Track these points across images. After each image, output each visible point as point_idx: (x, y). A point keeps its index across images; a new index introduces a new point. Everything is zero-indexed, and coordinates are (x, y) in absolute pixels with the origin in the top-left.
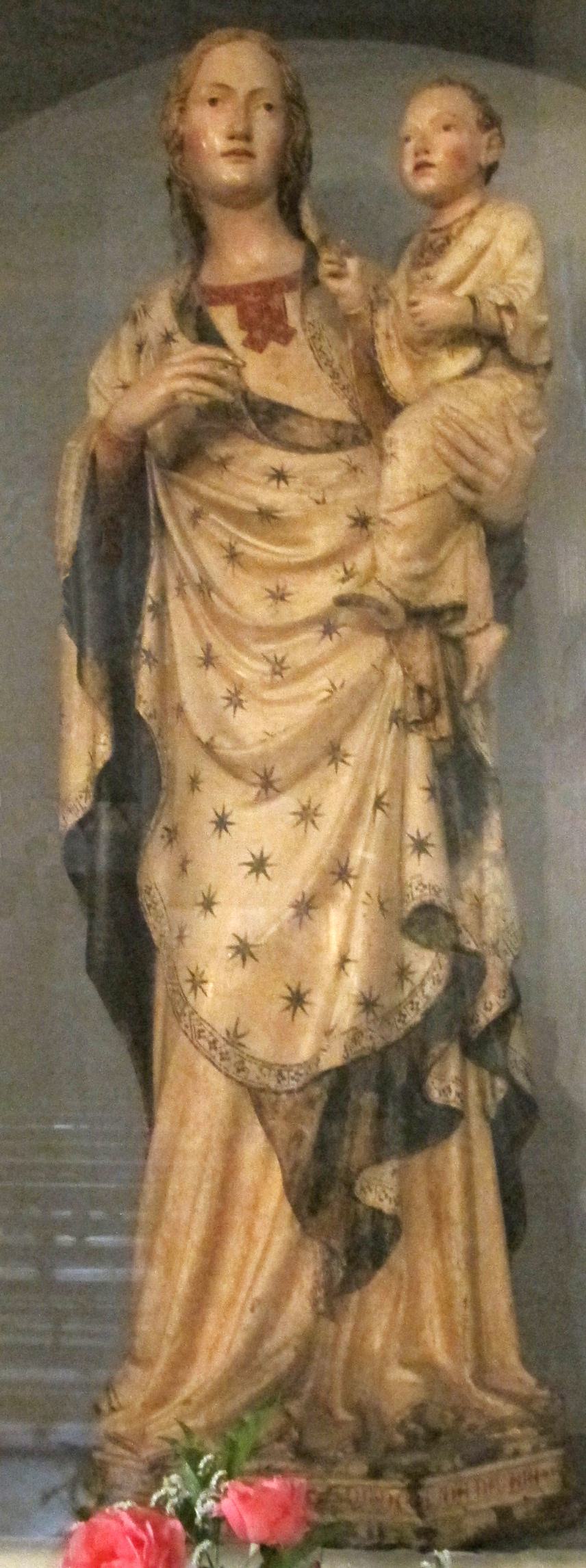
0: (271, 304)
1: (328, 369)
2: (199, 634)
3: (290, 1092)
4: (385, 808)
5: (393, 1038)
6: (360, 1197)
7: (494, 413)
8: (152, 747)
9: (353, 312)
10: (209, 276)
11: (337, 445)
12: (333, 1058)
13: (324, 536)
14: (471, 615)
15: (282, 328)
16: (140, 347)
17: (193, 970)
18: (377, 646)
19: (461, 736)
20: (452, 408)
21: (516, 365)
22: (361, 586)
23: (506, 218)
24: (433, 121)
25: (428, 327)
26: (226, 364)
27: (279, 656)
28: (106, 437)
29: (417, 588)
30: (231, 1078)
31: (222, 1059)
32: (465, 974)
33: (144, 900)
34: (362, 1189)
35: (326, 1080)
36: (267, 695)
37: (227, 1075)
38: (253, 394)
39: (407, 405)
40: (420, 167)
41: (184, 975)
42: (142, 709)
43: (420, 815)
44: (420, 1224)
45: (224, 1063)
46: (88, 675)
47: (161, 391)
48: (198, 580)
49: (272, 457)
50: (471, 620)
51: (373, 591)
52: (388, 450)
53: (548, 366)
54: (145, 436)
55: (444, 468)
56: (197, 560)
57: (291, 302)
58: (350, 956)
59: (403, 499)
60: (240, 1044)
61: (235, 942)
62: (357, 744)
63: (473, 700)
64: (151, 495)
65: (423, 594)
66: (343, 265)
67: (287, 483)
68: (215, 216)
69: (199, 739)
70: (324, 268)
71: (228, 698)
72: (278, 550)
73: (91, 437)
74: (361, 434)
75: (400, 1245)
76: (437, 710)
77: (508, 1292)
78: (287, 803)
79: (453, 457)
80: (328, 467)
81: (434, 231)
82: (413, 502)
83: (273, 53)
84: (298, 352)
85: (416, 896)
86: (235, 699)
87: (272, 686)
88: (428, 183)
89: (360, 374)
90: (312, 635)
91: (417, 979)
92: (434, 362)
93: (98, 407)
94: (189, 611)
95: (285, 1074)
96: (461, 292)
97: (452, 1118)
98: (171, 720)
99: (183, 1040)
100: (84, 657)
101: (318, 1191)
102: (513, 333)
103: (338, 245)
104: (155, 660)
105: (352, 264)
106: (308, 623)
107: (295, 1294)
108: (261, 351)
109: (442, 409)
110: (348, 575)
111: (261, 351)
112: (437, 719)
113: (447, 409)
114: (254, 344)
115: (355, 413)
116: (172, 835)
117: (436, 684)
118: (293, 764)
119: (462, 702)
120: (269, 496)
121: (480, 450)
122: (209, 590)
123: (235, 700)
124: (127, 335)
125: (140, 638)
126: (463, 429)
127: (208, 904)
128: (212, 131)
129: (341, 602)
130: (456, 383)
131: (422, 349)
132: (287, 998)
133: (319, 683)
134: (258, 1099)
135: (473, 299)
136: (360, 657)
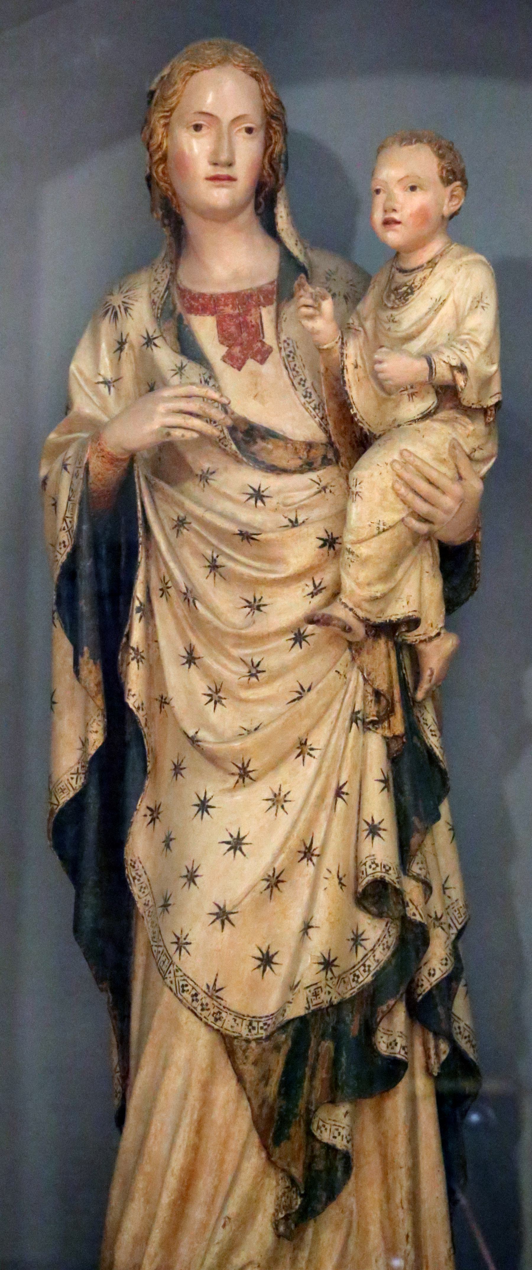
0: (249, 318)
2: (182, 633)
3: (258, 1040)
4: (344, 796)
5: (348, 996)
6: (317, 1134)
7: (445, 456)
9: (325, 347)
11: (309, 466)
12: (297, 1009)
14: (420, 630)
15: (259, 344)
16: (121, 345)
17: (178, 933)
19: (413, 728)
27: (256, 661)
30: (210, 1026)
31: (202, 1010)
32: (412, 940)
33: (130, 872)
34: (318, 1128)
35: (290, 1029)
36: (244, 694)
37: (206, 1024)
39: (376, 438)
40: (387, 223)
41: (169, 938)
42: (132, 702)
43: (378, 805)
44: (368, 1168)
45: (205, 1013)
46: (84, 673)
48: (184, 590)
51: (339, 612)
52: (354, 489)
55: (400, 506)
57: (267, 314)
58: (313, 923)
60: (218, 997)
61: (216, 910)
62: (317, 740)
64: (139, 503)
65: (382, 611)
67: (263, 502)
69: (185, 733)
75: (351, 1185)
76: (390, 711)
77: (448, 1238)
78: (261, 791)
79: (410, 496)
80: (297, 488)
84: (271, 370)
85: (370, 874)
86: (215, 697)
87: (249, 686)
91: (369, 945)
95: (255, 1024)
97: (394, 1071)
99: (167, 996)
100: (82, 655)
101: (279, 1123)
106: (280, 633)
107: (260, 1217)
108: (239, 369)
111: (239, 369)
112: (391, 719)
113: (405, 453)
116: (154, 814)
118: (267, 758)
125: (128, 636)
127: (191, 877)
132: (259, 959)
134: (229, 1045)
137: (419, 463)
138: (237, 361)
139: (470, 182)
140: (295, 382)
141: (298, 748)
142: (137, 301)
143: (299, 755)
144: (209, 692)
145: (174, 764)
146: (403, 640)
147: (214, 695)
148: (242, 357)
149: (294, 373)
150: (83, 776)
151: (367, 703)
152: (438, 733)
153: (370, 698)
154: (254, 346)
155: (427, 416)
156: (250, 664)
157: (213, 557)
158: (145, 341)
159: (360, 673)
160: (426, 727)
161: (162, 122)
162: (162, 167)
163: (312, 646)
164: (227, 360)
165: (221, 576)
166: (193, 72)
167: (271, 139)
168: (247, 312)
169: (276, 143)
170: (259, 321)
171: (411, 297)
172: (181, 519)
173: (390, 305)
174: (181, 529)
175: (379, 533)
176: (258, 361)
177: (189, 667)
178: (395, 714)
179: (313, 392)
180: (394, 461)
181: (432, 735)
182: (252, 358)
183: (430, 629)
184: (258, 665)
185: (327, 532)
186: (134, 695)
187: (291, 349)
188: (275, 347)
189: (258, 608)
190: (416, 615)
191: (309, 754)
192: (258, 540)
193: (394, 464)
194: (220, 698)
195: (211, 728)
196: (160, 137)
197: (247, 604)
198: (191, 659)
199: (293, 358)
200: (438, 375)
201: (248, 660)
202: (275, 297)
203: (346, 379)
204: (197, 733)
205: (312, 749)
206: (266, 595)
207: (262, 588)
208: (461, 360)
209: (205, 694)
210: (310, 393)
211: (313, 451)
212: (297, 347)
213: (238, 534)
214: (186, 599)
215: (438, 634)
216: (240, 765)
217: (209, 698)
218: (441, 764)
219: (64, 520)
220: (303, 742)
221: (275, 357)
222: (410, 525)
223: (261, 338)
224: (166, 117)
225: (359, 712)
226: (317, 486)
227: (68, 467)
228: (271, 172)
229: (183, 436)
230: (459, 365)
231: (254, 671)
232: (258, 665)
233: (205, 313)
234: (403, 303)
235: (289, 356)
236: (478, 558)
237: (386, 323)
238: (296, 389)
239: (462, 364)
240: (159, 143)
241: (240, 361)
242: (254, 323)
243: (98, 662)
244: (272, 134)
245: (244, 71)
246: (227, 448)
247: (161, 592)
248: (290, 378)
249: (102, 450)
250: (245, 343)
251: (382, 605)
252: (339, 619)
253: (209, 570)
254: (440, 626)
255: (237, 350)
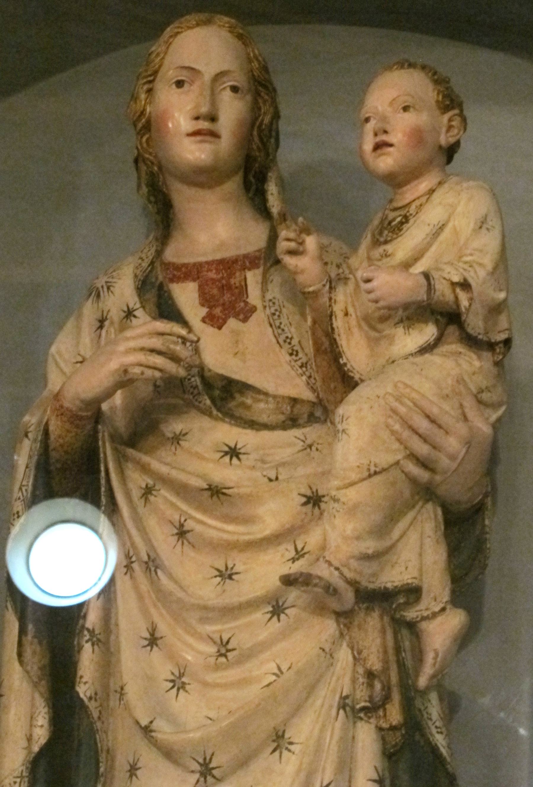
0: (232, 281)
1: (287, 346)
2: (145, 612)
8: (92, 732)
9: (311, 289)
10: (171, 254)
11: (292, 422)
13: (275, 512)
14: (422, 605)
16: (102, 322)
18: (329, 627)
19: (413, 723)
20: (406, 386)
21: (472, 342)
22: (311, 565)
23: (464, 196)
24: (396, 102)
25: (381, 304)
26: (184, 340)
28: (60, 411)
29: (368, 568)
38: (210, 370)
39: (362, 381)
42: (83, 690)
47: (114, 365)
48: (146, 558)
49: (227, 433)
50: (428, 604)
51: (323, 571)
53: (507, 342)
54: (99, 409)
55: (396, 445)
56: (148, 541)
57: (253, 278)
59: (354, 476)
62: (303, 731)
63: (428, 689)
65: (375, 575)
66: (302, 243)
67: (239, 459)
68: (183, 196)
69: (138, 723)
70: (282, 245)
71: (172, 681)
72: (231, 528)
73: (45, 411)
74: (318, 413)
76: (387, 698)
79: (406, 434)
80: (284, 443)
81: (395, 209)
82: (364, 479)
83: (240, 37)
84: (255, 331)
86: (178, 684)
87: (217, 668)
88: (385, 163)
89: (318, 349)
90: (260, 615)
92: (391, 339)
93: (55, 381)
94: (136, 588)
96: (419, 268)
98: (113, 701)
100: (26, 635)
102: (468, 310)
103: (296, 224)
104: (99, 640)
105: (311, 242)
108: (220, 328)
109: (395, 386)
110: (299, 554)
111: (220, 328)
112: (387, 706)
113: (399, 385)
114: (214, 321)
115: (313, 390)
117: (386, 669)
119: (417, 691)
120: (225, 474)
121: (436, 430)
122: (157, 567)
123: (178, 684)
124: (89, 312)
126: (415, 404)
128: (178, 111)
129: (288, 581)
130: (411, 359)
131: (379, 326)
133: (263, 669)
135: (427, 276)
136: (308, 638)
137: (414, 395)
138: (218, 320)
139: (467, 130)
140: (281, 340)
141: (274, 741)
142: (119, 279)
143: (274, 751)
144: (172, 678)
145: (130, 764)
146: (401, 616)
147: (177, 681)
148: (224, 317)
149: (280, 331)
150: (26, 780)
151: (357, 687)
152: (444, 730)
153: (361, 680)
154: (237, 305)
155: (426, 349)
156: (219, 641)
157: (180, 522)
158: (124, 314)
159: (350, 652)
160: (430, 723)
161: (146, 87)
162: (147, 136)
163: (292, 620)
164: (207, 320)
165: (189, 543)
166: (178, 33)
167: (259, 109)
168: (231, 275)
169: (265, 113)
170: (243, 283)
171: (405, 227)
172: (149, 486)
173: (382, 239)
174: (149, 496)
175: (370, 476)
176: (240, 320)
177: (151, 650)
178: (392, 700)
179: (300, 351)
180: (387, 393)
181: (438, 732)
182: (233, 317)
183: (433, 603)
184: (228, 642)
185: (311, 488)
186: (86, 683)
187: (277, 307)
188: (259, 306)
189: (230, 577)
190: (416, 582)
191: (287, 749)
192: (230, 496)
193: (387, 396)
194: (184, 683)
195: (172, 719)
196: (143, 102)
197: (218, 573)
198: (153, 640)
199: (279, 316)
200: (437, 293)
201: (216, 637)
202: (262, 262)
203: (335, 326)
204: (151, 722)
205: (291, 743)
206: (239, 562)
207: (234, 553)
208: (463, 275)
209: (167, 680)
210: (297, 352)
211: (298, 406)
212: (284, 306)
213: (206, 489)
214: (148, 568)
215: (443, 609)
216: (201, 761)
217: (171, 685)
218: (449, 766)
219: (20, 489)
220: (280, 733)
221: (259, 317)
222: (406, 470)
223: (245, 298)
224: (150, 82)
225: (347, 697)
226: (302, 443)
227: (30, 435)
228: (260, 145)
229: (142, 373)
230: (462, 281)
231: (223, 651)
232: (228, 642)
233: (187, 279)
234: (397, 234)
235: (274, 314)
236: (487, 530)
237: (380, 260)
238: (281, 347)
239: (465, 280)
240: (142, 109)
241: (221, 321)
242: (237, 285)
243: (45, 642)
244: (261, 105)
245: (230, 32)
246: (201, 405)
247: (125, 570)
248: (275, 336)
249: (62, 407)
250: (227, 303)
251: (374, 566)
252: (320, 578)
253: (176, 537)
254: (445, 600)
255: (218, 311)
